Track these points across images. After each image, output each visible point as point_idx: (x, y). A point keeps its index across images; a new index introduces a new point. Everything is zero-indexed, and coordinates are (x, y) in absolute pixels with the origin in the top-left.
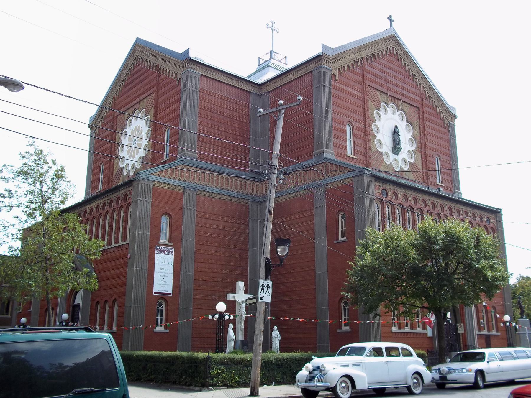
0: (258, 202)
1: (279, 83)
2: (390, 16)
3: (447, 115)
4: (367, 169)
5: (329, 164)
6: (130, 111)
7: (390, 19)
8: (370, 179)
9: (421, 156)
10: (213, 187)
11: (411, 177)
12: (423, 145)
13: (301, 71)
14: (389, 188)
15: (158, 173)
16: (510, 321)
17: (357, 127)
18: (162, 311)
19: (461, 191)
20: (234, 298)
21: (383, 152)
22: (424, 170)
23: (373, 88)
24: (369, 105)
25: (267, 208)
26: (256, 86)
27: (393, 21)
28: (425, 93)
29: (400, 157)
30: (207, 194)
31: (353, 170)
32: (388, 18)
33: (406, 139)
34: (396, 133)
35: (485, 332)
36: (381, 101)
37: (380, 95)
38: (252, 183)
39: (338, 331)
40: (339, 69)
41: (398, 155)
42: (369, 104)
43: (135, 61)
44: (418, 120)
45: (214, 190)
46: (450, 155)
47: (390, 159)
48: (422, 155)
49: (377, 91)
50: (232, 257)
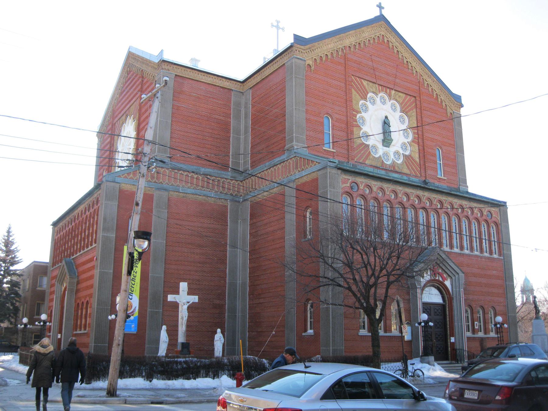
0: (239, 202)
1: (259, 78)
2: (380, 3)
3: (451, 104)
5: (299, 158)
6: (124, 117)
7: (380, 7)
8: (336, 172)
9: (418, 147)
10: (187, 187)
11: (406, 171)
12: (420, 136)
13: (277, 64)
14: (360, 182)
15: (126, 175)
19: (468, 184)
20: (175, 299)
21: (371, 145)
22: (422, 163)
23: (358, 77)
24: (353, 96)
25: (135, 199)
26: (239, 83)
27: (383, 8)
28: (423, 81)
29: (391, 150)
30: (180, 195)
31: (319, 163)
32: (377, 6)
34: (386, 123)
35: (481, 334)
36: (368, 91)
38: (237, 184)
39: (303, 334)
40: (315, 59)
41: (389, 147)
42: (353, 94)
43: (128, 69)
44: (415, 110)
45: (189, 191)
46: (454, 145)
47: (381, 150)
48: (419, 147)
49: (357, 78)
50: (208, 258)
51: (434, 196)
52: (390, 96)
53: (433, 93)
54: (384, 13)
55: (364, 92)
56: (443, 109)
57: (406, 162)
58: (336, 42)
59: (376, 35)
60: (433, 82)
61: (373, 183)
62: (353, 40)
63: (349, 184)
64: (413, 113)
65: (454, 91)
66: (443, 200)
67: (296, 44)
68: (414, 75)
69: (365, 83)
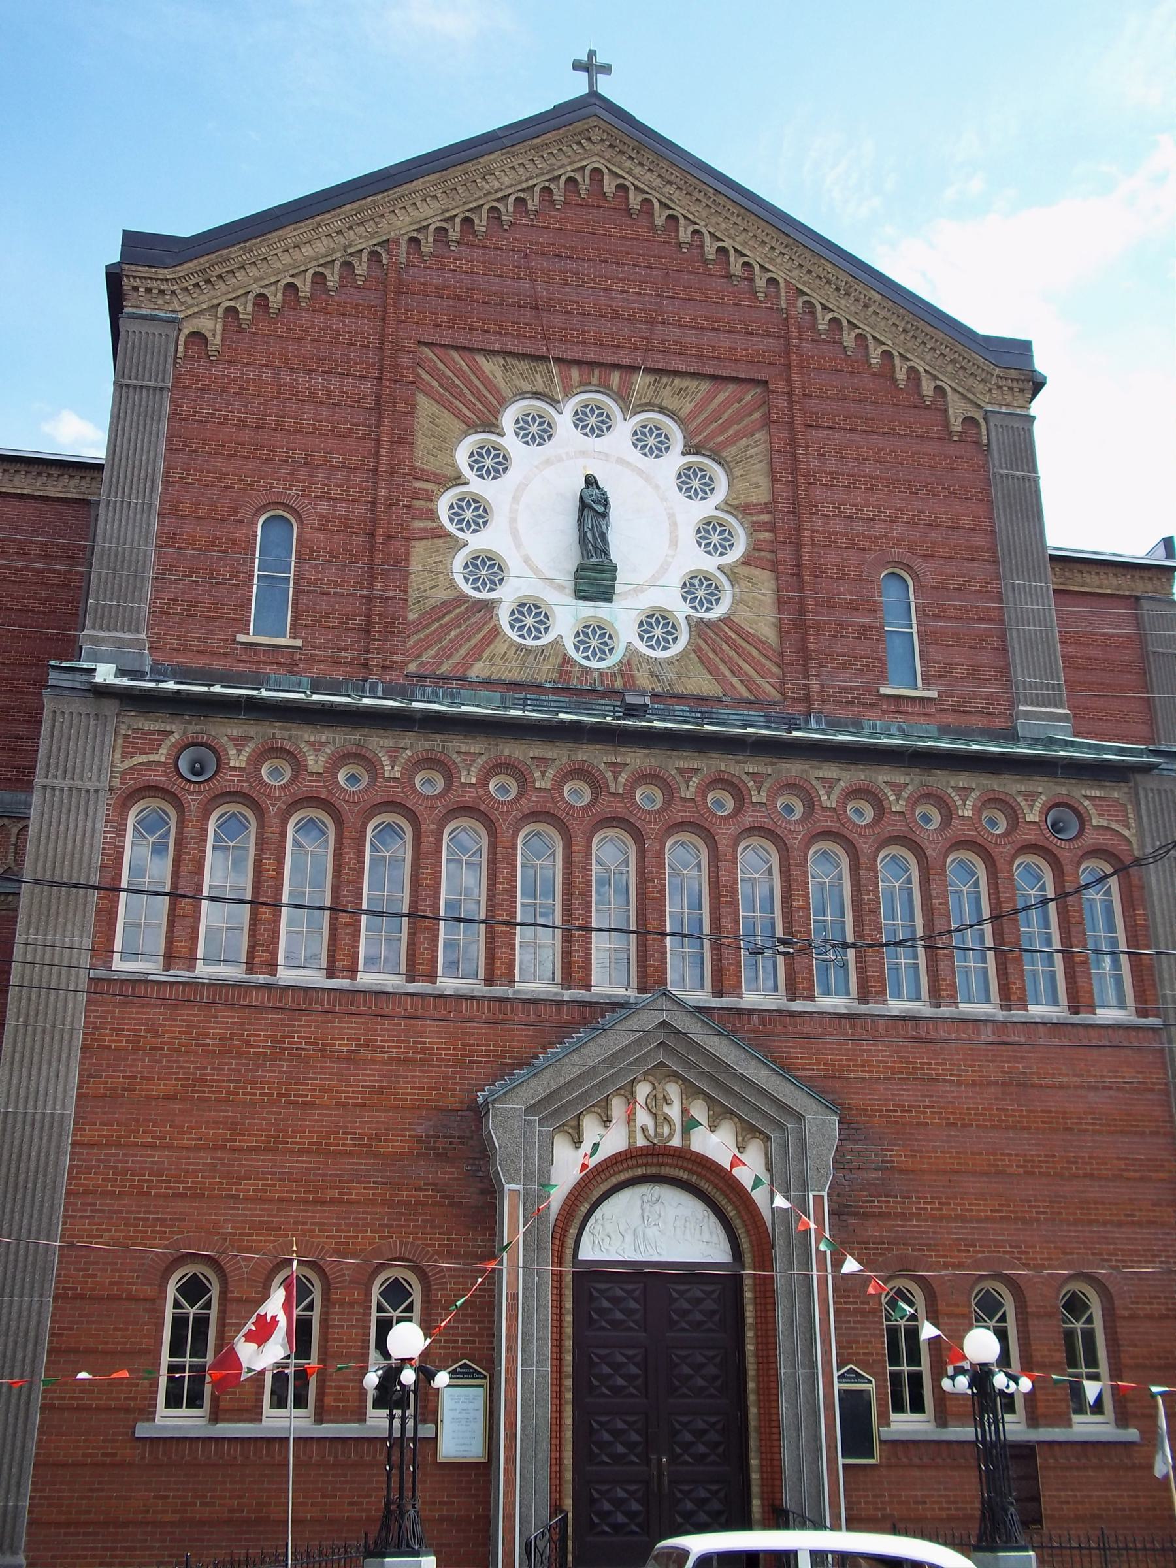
4: (65, 664)
7: (589, 66)
16: (425, 1354)
17: (322, 517)
18: (1089, 1336)
23: (457, 348)
33: (674, 524)
36: (506, 391)
37: (499, 374)
49: (455, 355)
51: (682, 764)
52: (622, 398)
53: (867, 356)
54: (606, 87)
55: (480, 397)
56: (928, 408)
57: (698, 651)
58: (339, 232)
59: (557, 173)
60: (866, 306)
61: (306, 737)
62: (431, 213)
63: (163, 751)
64: (756, 446)
65: (984, 323)
66: (744, 777)
67: (133, 267)
68: (761, 295)
69: (490, 366)
